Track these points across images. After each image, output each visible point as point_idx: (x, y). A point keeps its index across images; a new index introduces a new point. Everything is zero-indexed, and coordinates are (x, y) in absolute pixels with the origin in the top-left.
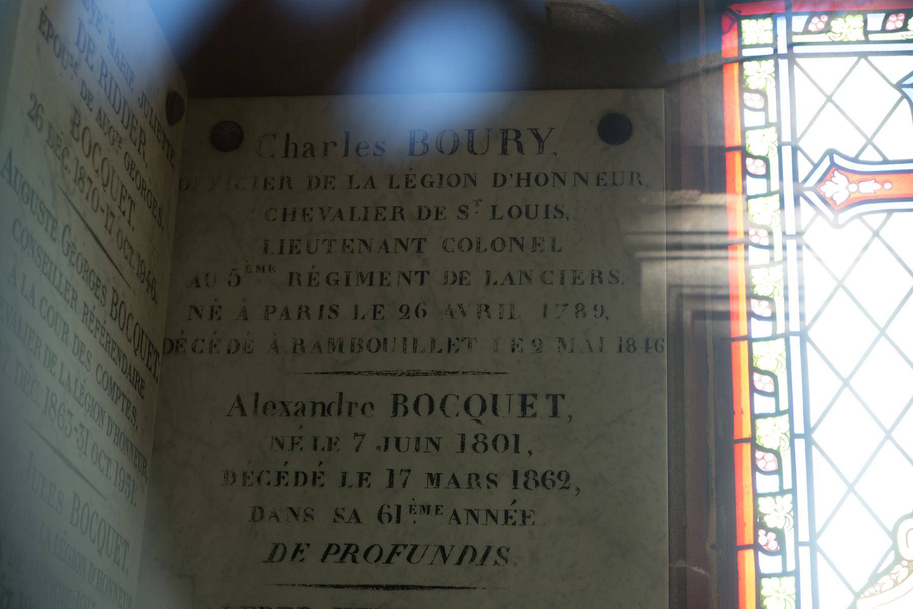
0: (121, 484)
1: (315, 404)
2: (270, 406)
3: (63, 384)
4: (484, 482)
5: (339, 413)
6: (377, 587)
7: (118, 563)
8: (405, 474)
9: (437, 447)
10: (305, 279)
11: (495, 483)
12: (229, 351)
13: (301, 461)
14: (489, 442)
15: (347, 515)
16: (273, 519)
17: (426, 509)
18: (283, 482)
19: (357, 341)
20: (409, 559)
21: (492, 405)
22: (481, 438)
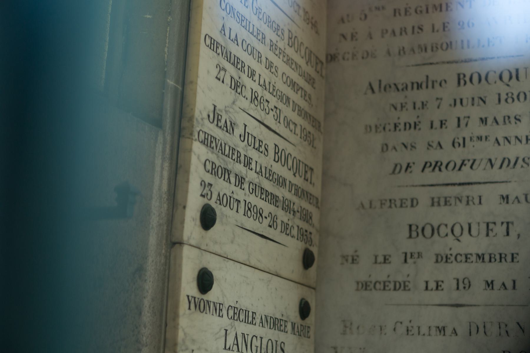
0: (305, 137)
1: (413, 83)
2: (388, 87)
3: (261, 86)
4: (513, 120)
5: (427, 87)
6: (454, 184)
7: (307, 180)
8: (466, 119)
9: (484, 102)
10: (403, 12)
11: (519, 120)
12: (363, 58)
13: (407, 116)
14: (515, 97)
15: (435, 145)
16: (394, 150)
17: (480, 138)
18: (398, 129)
19: (434, 45)
20: (471, 167)
21: (254, 98)
22: (510, 95)
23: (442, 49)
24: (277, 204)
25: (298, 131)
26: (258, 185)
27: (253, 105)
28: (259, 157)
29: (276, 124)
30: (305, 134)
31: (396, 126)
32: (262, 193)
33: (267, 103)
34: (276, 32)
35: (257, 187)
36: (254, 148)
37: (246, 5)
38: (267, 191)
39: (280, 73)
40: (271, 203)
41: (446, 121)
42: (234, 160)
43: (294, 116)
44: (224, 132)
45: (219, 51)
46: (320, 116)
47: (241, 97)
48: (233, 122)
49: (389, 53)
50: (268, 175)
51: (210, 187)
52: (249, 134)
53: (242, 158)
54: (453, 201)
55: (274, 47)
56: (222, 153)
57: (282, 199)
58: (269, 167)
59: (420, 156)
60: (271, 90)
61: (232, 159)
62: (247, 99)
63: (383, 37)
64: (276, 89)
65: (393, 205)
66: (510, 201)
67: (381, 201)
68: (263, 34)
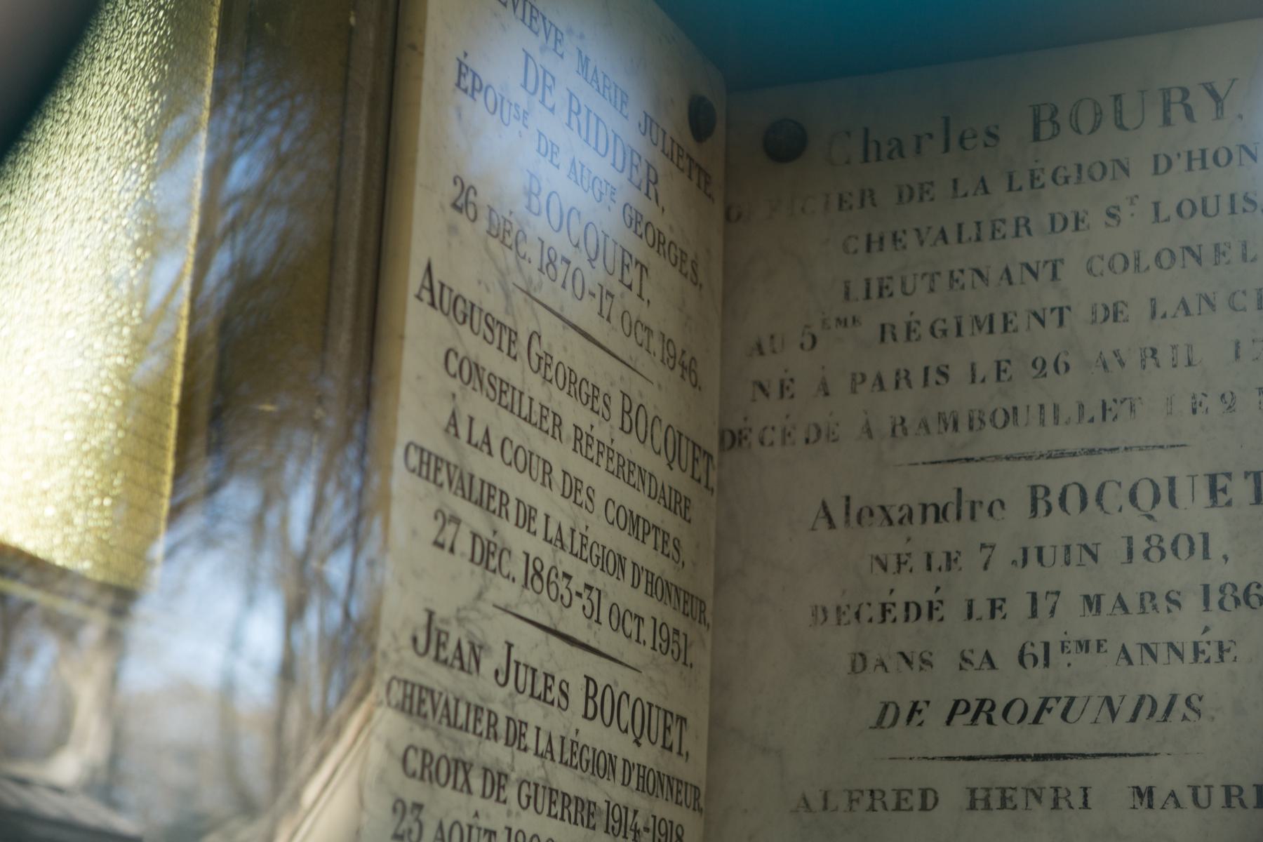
1: (925, 507)
2: (866, 513)
3: (550, 542)
4: (1162, 603)
5: (959, 517)
6: (1023, 757)
8: (1052, 598)
9: (1095, 558)
10: (901, 333)
11: (1178, 604)
12: (807, 441)
14: (1167, 545)
15: (977, 658)
16: (880, 669)
18: (889, 617)
19: (976, 415)
20: (1064, 716)
21: (535, 574)
22: (1155, 541)
23: (995, 426)
24: (592, 822)
25: (647, 633)
26: (541, 783)
27: (529, 594)
28: (545, 716)
29: (589, 627)
30: (665, 636)
31: (884, 610)
32: (552, 803)
33: (566, 581)
34: (590, 405)
35: (540, 790)
36: (532, 695)
37: (513, 353)
38: (564, 794)
39: (599, 501)
40: (575, 823)
41: (1004, 600)
42: (481, 734)
43: (636, 600)
44: (455, 671)
45: (443, 477)
46: (704, 586)
47: (498, 579)
48: (477, 643)
49: (869, 432)
50: (567, 756)
51: (416, 812)
52: (518, 664)
53: (502, 726)
54: (1019, 798)
55: (584, 442)
56: (449, 724)
57: (604, 806)
58: (572, 735)
59: (943, 685)
60: (577, 547)
61: (474, 732)
62: (514, 580)
63: (854, 391)
64: (590, 542)
65: (878, 805)
66: (1157, 803)
67: (851, 792)
68: (555, 414)
